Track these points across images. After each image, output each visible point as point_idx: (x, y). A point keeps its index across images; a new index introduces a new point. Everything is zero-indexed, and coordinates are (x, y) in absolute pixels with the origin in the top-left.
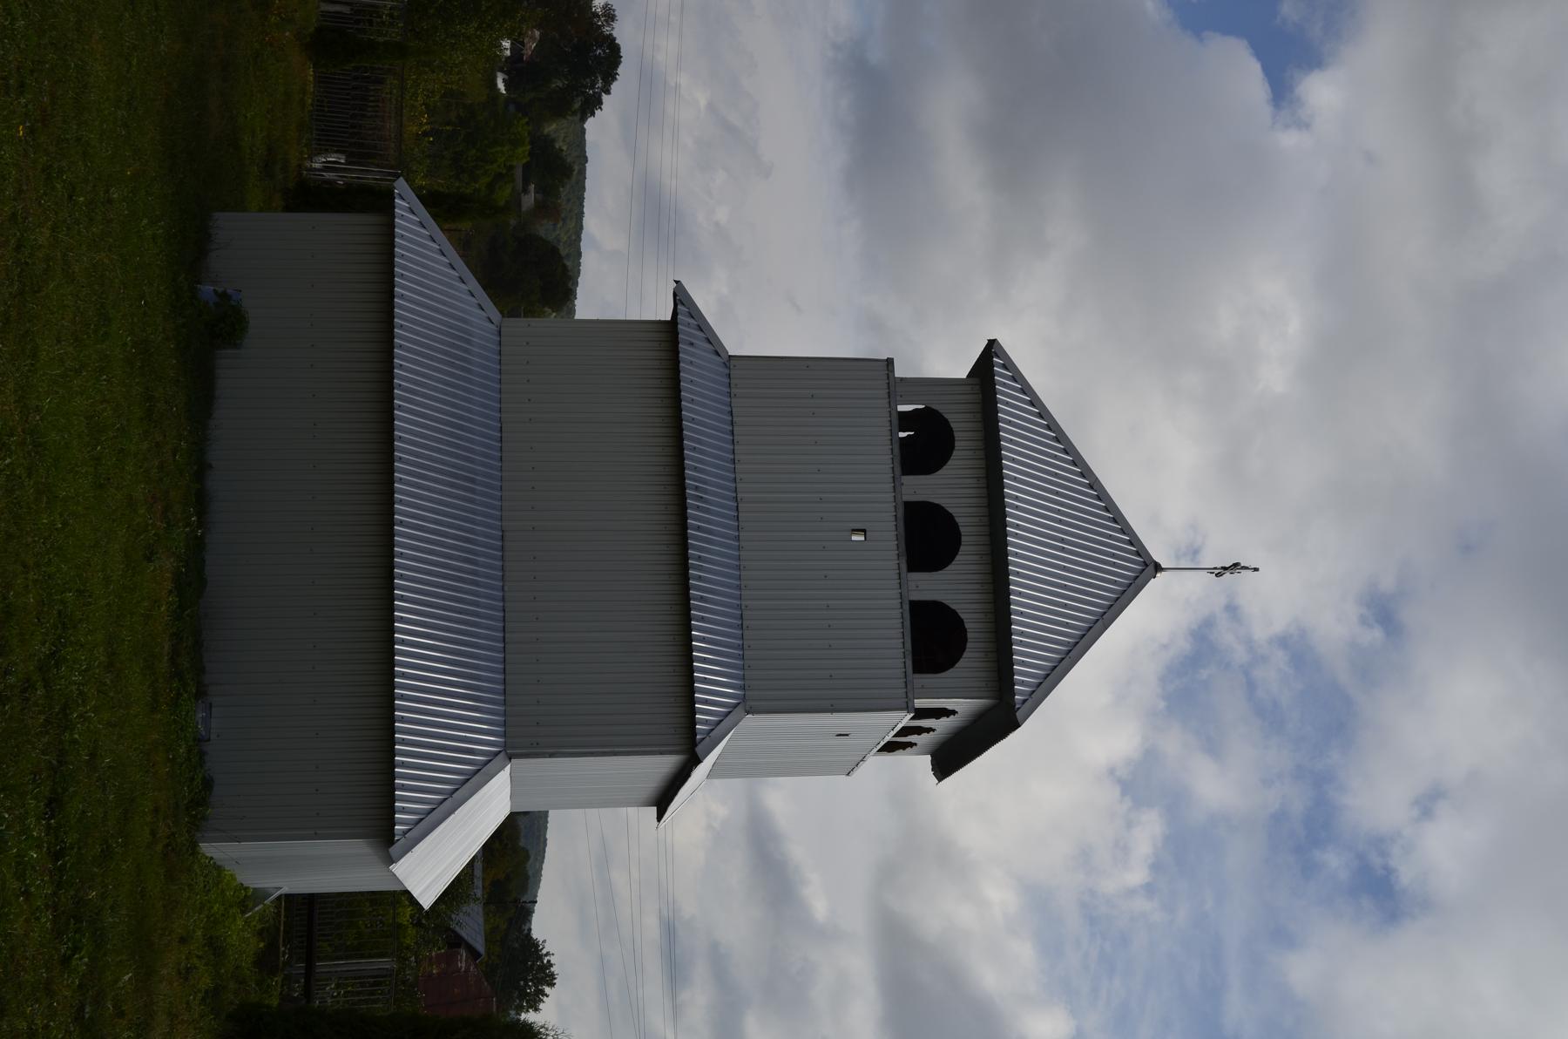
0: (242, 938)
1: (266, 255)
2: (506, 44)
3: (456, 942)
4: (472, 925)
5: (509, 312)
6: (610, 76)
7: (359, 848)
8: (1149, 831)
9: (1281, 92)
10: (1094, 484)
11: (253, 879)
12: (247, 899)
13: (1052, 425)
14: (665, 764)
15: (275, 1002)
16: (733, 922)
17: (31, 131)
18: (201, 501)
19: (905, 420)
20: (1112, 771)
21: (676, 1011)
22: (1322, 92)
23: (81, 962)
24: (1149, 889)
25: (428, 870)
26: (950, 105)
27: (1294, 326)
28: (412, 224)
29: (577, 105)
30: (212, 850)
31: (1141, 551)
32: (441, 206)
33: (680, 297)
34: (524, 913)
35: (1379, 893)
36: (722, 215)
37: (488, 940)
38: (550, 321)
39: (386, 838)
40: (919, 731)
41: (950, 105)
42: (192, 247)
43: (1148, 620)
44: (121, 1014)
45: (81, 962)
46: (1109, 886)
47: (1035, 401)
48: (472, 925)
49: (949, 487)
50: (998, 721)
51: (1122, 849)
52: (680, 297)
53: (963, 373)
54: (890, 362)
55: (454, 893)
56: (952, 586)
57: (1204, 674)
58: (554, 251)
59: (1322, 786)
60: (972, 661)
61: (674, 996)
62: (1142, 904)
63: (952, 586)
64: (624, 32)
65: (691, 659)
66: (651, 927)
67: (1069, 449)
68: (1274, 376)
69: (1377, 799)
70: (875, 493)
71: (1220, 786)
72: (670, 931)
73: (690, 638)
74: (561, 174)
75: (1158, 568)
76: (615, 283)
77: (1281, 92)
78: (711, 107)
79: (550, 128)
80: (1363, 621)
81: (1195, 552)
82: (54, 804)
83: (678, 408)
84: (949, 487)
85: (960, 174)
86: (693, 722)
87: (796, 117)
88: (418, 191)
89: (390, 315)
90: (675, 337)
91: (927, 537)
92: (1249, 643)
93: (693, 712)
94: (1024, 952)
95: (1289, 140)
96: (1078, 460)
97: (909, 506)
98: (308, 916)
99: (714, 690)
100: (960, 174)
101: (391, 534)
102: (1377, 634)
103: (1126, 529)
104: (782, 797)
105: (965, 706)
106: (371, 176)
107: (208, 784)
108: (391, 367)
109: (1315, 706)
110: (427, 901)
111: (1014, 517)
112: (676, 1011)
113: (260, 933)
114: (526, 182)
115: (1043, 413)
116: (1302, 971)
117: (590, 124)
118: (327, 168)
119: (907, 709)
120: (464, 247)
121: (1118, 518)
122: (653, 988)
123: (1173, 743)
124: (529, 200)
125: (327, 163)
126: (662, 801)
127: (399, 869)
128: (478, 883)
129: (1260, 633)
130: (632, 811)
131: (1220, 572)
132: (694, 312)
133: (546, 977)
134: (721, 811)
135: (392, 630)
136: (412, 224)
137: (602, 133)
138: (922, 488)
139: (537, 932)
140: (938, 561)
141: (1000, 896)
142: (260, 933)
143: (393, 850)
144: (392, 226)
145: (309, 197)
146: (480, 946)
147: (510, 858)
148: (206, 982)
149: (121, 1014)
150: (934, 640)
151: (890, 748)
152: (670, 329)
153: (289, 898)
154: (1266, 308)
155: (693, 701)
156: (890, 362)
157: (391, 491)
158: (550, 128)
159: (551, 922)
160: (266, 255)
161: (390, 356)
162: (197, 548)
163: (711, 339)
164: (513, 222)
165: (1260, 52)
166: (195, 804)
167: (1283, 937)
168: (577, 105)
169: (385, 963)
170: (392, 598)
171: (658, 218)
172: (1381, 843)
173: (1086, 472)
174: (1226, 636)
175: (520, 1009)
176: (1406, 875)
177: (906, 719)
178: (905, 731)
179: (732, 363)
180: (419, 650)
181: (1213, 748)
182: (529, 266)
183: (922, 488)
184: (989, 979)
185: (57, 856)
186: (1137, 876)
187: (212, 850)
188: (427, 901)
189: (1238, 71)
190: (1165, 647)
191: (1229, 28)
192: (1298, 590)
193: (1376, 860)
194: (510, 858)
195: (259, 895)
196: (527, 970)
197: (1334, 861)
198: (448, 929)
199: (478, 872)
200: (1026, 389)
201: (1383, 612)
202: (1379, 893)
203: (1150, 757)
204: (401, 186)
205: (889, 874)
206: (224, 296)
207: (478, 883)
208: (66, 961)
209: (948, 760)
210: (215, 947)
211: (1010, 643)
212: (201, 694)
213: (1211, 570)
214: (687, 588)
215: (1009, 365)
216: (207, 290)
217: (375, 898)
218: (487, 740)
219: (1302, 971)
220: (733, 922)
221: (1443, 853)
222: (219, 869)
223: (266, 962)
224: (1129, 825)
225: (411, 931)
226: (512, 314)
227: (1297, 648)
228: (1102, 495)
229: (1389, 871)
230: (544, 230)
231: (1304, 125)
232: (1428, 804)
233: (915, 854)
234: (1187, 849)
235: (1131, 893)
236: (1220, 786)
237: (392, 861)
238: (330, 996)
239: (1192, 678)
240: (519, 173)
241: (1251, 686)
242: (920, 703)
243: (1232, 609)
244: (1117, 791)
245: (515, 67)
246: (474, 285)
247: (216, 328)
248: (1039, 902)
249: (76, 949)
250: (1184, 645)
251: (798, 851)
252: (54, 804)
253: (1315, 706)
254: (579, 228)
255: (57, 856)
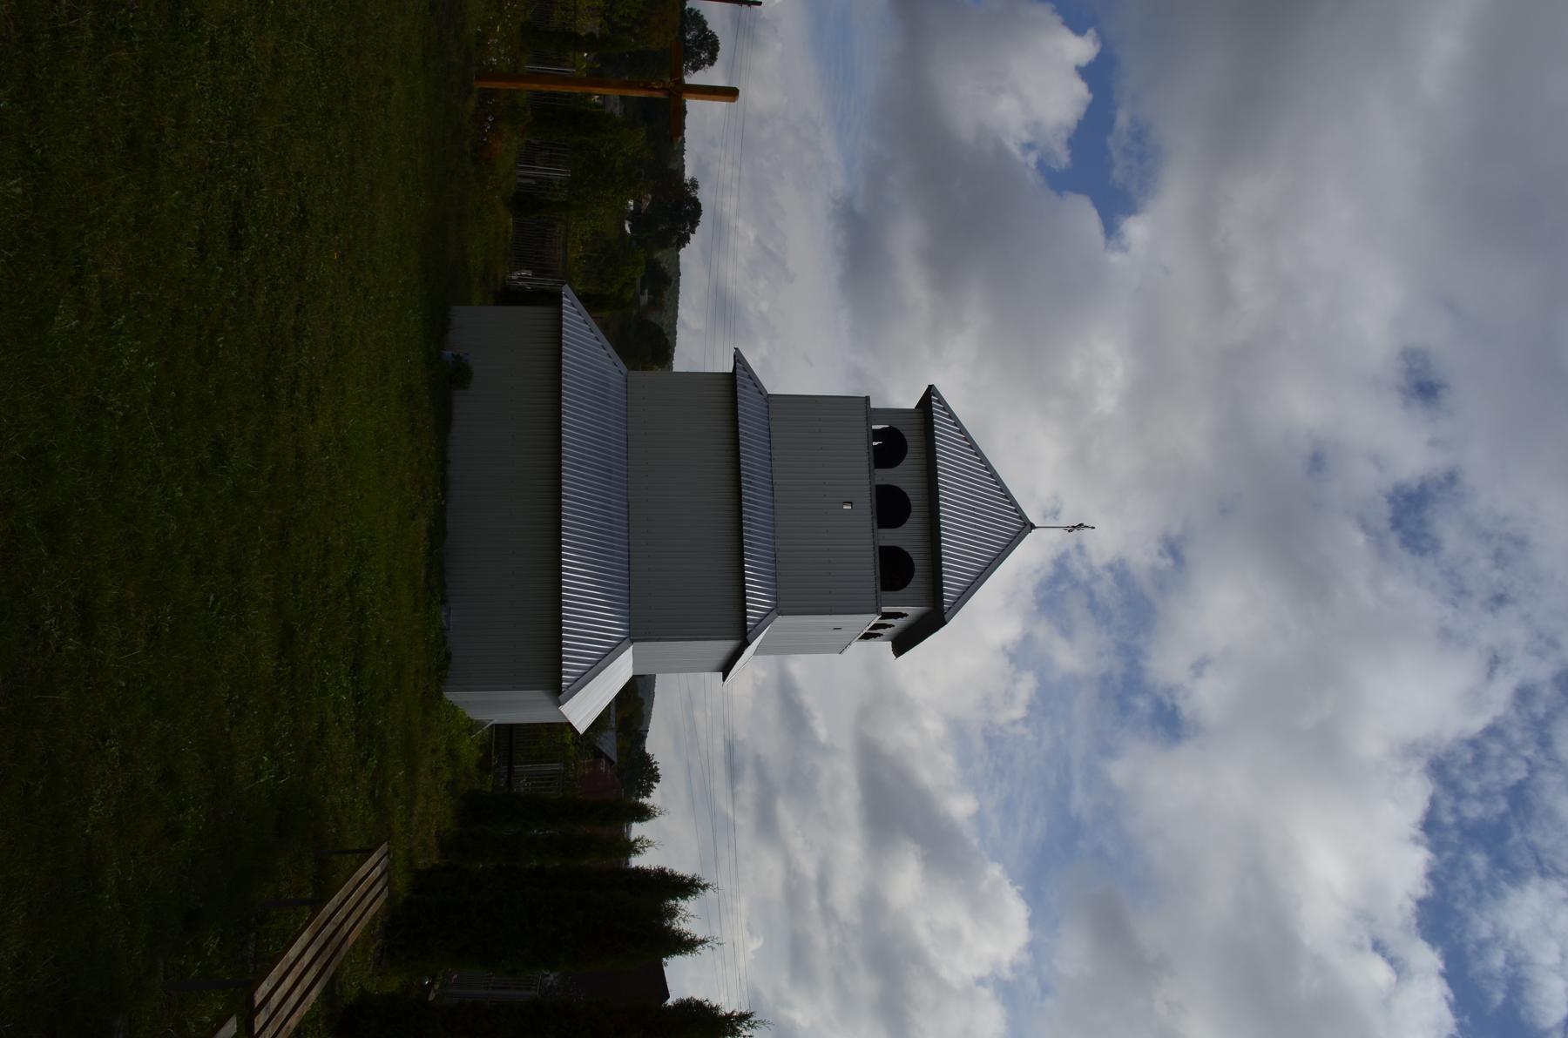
0: (469, 750)
1: (482, 331)
2: (631, 203)
3: (599, 754)
4: (609, 744)
5: (631, 368)
6: (695, 223)
7: (539, 695)
8: (1026, 686)
9: (1111, 229)
10: (994, 474)
11: (477, 715)
12: (473, 726)
13: (968, 438)
14: (728, 646)
15: (489, 789)
16: (769, 743)
17: (342, 256)
18: (444, 483)
19: (877, 435)
20: (1004, 648)
21: (734, 796)
22: (1136, 229)
23: (373, 763)
24: (1026, 721)
25: (583, 710)
26: (906, 237)
27: (1119, 372)
28: (573, 314)
29: (674, 240)
30: (450, 696)
31: (1022, 516)
32: (591, 302)
33: (738, 358)
34: (641, 737)
35: (1169, 723)
36: (764, 306)
37: (619, 753)
38: (655, 375)
39: (557, 691)
40: (884, 626)
41: (906, 237)
42: (438, 328)
43: (1028, 556)
44: (397, 795)
45: (373, 763)
46: (1002, 718)
47: (957, 423)
48: (609, 744)
49: (904, 476)
50: (933, 620)
51: (1009, 697)
52: (738, 358)
53: (912, 405)
54: (867, 399)
55: (598, 725)
56: (905, 537)
57: (1062, 588)
58: (660, 330)
59: (1131, 655)
60: (918, 583)
61: (732, 787)
62: (1020, 730)
63: (905, 537)
64: (703, 195)
65: (744, 582)
66: (719, 746)
67: (978, 453)
68: (1107, 404)
69: (1167, 665)
70: (856, 482)
71: (1071, 657)
72: (730, 747)
73: (744, 569)
74: (664, 283)
75: (1033, 527)
76: (697, 349)
77: (1111, 229)
78: (757, 240)
79: (658, 255)
80: (1160, 554)
81: (1056, 514)
82: (356, 667)
83: (736, 427)
84: (904, 476)
85: (913, 283)
86: (745, 620)
87: (809, 244)
88: (576, 293)
89: (559, 370)
90: (735, 384)
91: (890, 508)
92: (1090, 568)
93: (745, 614)
94: (948, 761)
95: (1115, 258)
96: (984, 460)
97: (879, 488)
98: (510, 738)
99: (758, 600)
100: (913, 283)
101: (560, 504)
102: (1169, 561)
103: (1013, 502)
104: (799, 666)
105: (912, 611)
106: (548, 283)
107: (448, 656)
108: (560, 400)
109: (1127, 607)
110: (581, 729)
111: (942, 479)
112: (734, 796)
113: (480, 748)
114: (643, 288)
115: (962, 430)
116: (1118, 772)
117: (682, 252)
118: (520, 279)
119: (877, 612)
120: (604, 328)
121: (1008, 496)
122: (720, 782)
123: (1043, 630)
124: (645, 299)
125: (521, 276)
126: (726, 669)
127: (565, 709)
128: (613, 718)
129: (1098, 561)
130: (708, 675)
131: (1071, 529)
132: (747, 368)
133: (657, 778)
134: (762, 674)
135: (561, 563)
136: (573, 314)
137: (690, 257)
138: (887, 476)
139: (649, 749)
140: (895, 522)
141: (933, 726)
142: (480, 748)
143: (561, 697)
144: (561, 314)
145: (510, 296)
146: (614, 757)
147: (632, 704)
148: (447, 776)
149: (397, 795)
150: (894, 571)
151: (866, 637)
152: (731, 378)
153: (498, 726)
154: (1102, 362)
155: (745, 607)
156: (867, 399)
157: (560, 477)
158: (658, 255)
159: (657, 743)
160: (482, 331)
161: (560, 381)
162: (442, 511)
163: (757, 384)
164: (634, 312)
165: (1097, 205)
166: (441, 669)
167: (1108, 750)
168: (674, 240)
169: (556, 767)
170: (560, 543)
171: (724, 309)
172: (1171, 691)
173: (989, 467)
174: (1076, 564)
175: (638, 796)
176: (1186, 710)
177: (876, 619)
178: (876, 627)
179: (770, 398)
180: (579, 578)
181: (1067, 633)
182: (645, 341)
183: (887, 476)
184: (927, 777)
185: (358, 698)
186: (1018, 712)
187: (450, 696)
188: (581, 729)
189: (1083, 215)
190: (1037, 571)
191: (1078, 190)
192: (1119, 535)
193: (1167, 701)
194: (632, 704)
195: (480, 724)
196: (642, 772)
197: (1142, 703)
198: (594, 747)
199: (613, 712)
200: (952, 415)
201: (1173, 549)
202: (1169, 723)
203: (1027, 640)
204: (566, 289)
205: (865, 714)
206: (458, 357)
207: (613, 718)
208: (363, 762)
209: (902, 644)
210: (453, 755)
211: (941, 566)
212: (444, 601)
213: (1065, 528)
214: (741, 537)
215: (941, 400)
216: (448, 353)
217: (550, 727)
218: (619, 631)
219: (1118, 772)
220: (769, 743)
221: (1207, 697)
222: (455, 708)
223: (484, 765)
224: (1015, 681)
225: (572, 748)
226: (633, 369)
227: (1120, 571)
228: (999, 481)
229: (1175, 708)
230: (654, 317)
231: (1124, 249)
232: (1199, 667)
233: (882, 701)
234: (1051, 698)
235: (1014, 723)
236: (1071, 657)
237: (560, 704)
238: (523, 786)
239: (1057, 591)
240: (638, 282)
241: (1091, 595)
242: (885, 609)
243: (1080, 548)
244: (1007, 660)
245: (636, 218)
246: (610, 350)
247: (452, 377)
248: (958, 730)
249: (369, 755)
250: (1049, 570)
251: (809, 699)
252: (356, 667)
253: (1127, 607)
254: (676, 316)
255: (358, 698)
